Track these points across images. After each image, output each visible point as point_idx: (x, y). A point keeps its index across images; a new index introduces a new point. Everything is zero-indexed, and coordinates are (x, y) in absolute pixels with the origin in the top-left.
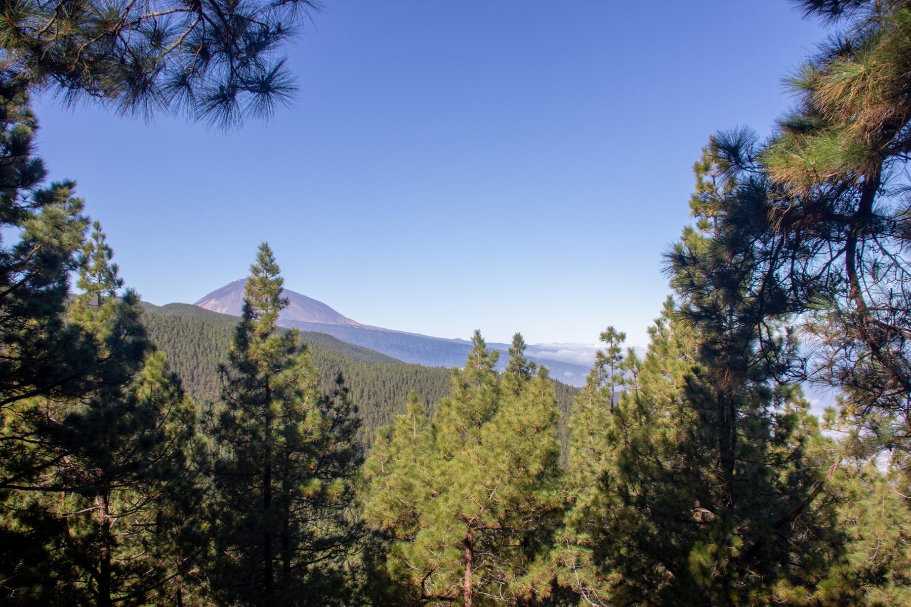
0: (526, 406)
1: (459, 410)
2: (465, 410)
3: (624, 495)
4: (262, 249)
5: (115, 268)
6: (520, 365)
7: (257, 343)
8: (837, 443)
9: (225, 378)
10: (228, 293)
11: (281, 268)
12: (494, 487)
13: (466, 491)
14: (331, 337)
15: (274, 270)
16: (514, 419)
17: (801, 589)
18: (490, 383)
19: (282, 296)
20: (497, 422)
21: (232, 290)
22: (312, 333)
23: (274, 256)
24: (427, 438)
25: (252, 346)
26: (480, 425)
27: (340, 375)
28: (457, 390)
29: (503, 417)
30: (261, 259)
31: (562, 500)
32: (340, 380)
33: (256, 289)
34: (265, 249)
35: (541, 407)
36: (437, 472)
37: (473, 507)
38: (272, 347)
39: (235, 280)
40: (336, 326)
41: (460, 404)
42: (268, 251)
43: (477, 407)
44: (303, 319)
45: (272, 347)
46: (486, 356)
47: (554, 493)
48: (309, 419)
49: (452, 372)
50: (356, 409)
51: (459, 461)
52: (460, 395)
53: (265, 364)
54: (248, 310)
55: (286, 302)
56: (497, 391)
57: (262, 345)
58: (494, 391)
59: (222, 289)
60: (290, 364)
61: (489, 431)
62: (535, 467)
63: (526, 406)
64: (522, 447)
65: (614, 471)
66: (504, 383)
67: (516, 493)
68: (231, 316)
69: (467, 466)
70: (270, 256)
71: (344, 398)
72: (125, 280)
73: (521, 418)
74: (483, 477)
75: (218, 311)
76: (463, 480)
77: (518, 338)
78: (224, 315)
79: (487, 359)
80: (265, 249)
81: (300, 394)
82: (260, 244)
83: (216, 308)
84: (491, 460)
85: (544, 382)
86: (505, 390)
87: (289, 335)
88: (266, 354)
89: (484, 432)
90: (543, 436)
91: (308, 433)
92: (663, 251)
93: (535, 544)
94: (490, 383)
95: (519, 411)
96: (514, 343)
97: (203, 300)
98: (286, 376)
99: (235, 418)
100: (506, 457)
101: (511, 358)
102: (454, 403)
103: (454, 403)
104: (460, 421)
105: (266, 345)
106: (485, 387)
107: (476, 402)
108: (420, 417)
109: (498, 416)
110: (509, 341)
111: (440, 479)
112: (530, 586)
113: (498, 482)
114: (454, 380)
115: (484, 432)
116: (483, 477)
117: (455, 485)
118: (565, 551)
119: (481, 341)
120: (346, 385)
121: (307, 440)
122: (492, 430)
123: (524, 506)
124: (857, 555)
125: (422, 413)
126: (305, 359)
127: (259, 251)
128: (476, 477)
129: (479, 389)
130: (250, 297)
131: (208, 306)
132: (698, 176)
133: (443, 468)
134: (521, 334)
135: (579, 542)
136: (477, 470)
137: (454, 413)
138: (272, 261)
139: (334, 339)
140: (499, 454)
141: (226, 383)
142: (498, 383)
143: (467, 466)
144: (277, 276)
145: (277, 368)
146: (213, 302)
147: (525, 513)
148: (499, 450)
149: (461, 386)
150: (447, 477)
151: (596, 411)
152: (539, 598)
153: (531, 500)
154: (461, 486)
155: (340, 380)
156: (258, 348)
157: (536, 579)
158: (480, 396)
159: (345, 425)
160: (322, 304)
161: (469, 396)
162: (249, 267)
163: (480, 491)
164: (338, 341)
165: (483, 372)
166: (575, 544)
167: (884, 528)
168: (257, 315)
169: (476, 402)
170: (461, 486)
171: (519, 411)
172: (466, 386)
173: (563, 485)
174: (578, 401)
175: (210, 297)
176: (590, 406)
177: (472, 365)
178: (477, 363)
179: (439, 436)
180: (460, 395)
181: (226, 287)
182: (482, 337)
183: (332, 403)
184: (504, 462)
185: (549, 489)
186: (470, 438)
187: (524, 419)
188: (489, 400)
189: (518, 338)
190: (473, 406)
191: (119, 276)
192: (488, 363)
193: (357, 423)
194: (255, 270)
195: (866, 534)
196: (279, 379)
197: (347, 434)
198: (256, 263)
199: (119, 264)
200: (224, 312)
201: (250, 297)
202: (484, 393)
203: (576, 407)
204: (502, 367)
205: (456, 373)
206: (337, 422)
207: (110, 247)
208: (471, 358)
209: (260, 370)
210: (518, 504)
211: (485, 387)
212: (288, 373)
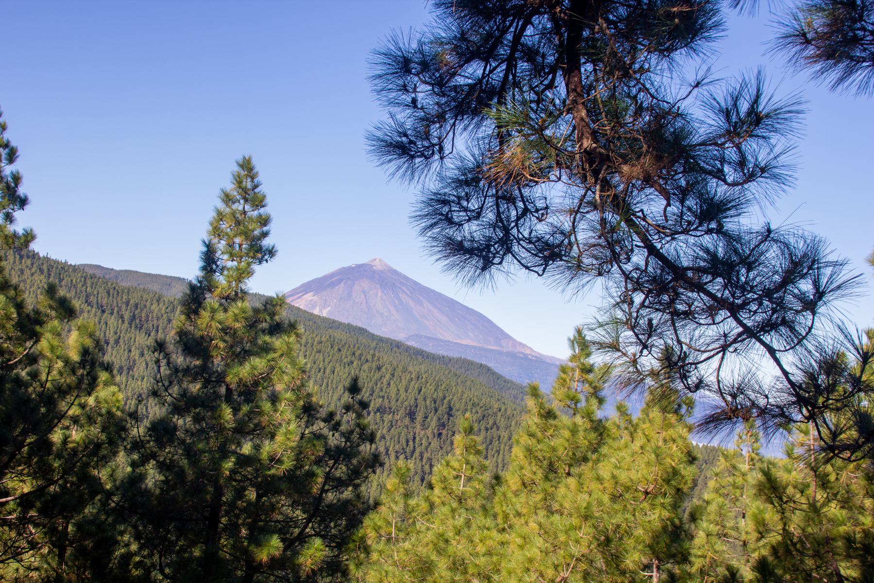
1: (529, 451)
4: (242, 166)
5: (17, 179)
7: (213, 311)
8: (570, 364)
9: (163, 363)
10: (333, 285)
11: (268, 200)
14: (489, 369)
15: (259, 202)
19: (266, 242)
21: (340, 281)
22: (458, 360)
23: (260, 178)
24: (478, 494)
25: (205, 315)
27: (355, 380)
28: (533, 421)
30: (239, 182)
32: (354, 388)
33: (224, 226)
34: (247, 166)
36: (481, 549)
38: (236, 320)
39: (347, 264)
40: (500, 353)
41: (531, 442)
42: (251, 169)
44: (448, 336)
45: (236, 320)
48: (279, 438)
49: (528, 390)
50: (372, 439)
53: (222, 345)
54: (209, 259)
55: (271, 252)
57: (221, 316)
59: (326, 278)
60: (266, 349)
61: (567, 492)
68: (334, 321)
70: (252, 178)
71: (359, 416)
72: (30, 197)
75: (316, 312)
78: (324, 320)
79: (590, 377)
80: (247, 166)
81: (274, 399)
82: (240, 158)
83: (314, 307)
87: (271, 305)
88: (225, 330)
90: (653, 506)
91: (274, 460)
97: (296, 292)
98: (254, 368)
99: (175, 428)
100: (586, 533)
105: (226, 318)
107: (560, 442)
108: (472, 458)
111: (482, 561)
114: (531, 403)
120: (364, 395)
121: (273, 471)
125: (478, 452)
126: (288, 344)
127: (236, 168)
130: (215, 241)
131: (302, 303)
133: (489, 543)
138: (256, 186)
139: (494, 373)
141: (164, 370)
144: (262, 211)
145: (242, 356)
146: (309, 296)
150: (495, 559)
155: (354, 388)
156: (212, 318)
158: (567, 434)
159: (353, 456)
160: (481, 316)
162: (218, 192)
164: (499, 377)
168: (223, 268)
172: (549, 415)
175: (306, 288)
179: (500, 490)
181: (332, 275)
183: (338, 424)
184: (582, 542)
190: (554, 449)
191: (22, 191)
193: (375, 462)
194: (228, 199)
196: (244, 371)
197: (355, 476)
198: (230, 186)
199: (23, 172)
200: (325, 313)
201: (215, 241)
205: (535, 392)
206: (337, 454)
207: (13, 144)
209: (214, 353)
212: (259, 363)
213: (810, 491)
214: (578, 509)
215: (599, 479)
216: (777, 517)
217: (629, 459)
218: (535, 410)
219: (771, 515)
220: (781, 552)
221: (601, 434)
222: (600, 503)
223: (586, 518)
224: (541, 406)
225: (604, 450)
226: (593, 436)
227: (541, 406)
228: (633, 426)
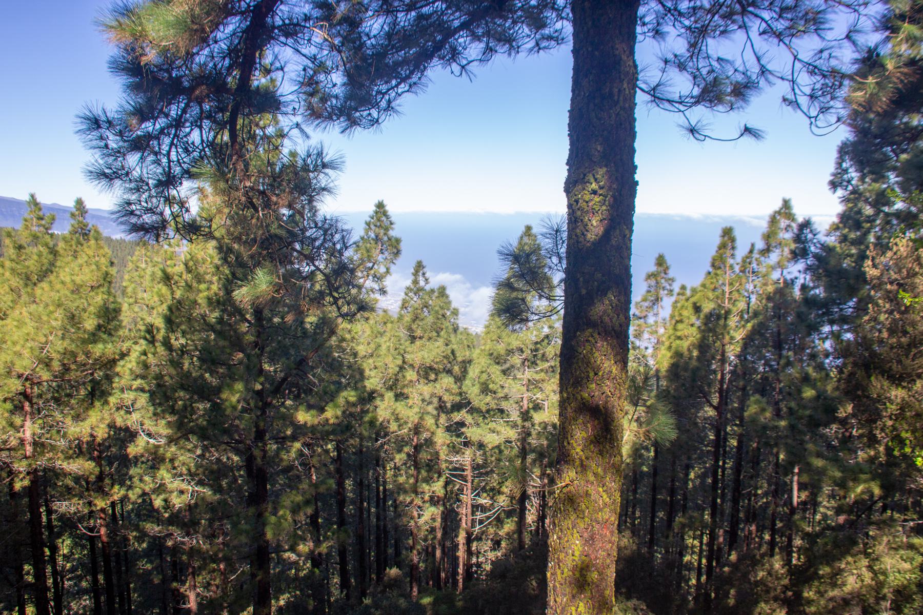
0: (81, 266)
1: (13, 270)
2: (19, 271)
3: (167, 344)
6: (82, 229)
12: (46, 343)
13: (18, 348)
16: (68, 279)
17: (313, 412)
18: (46, 245)
20: (51, 282)
26: (35, 284)
28: (12, 252)
29: (57, 277)
31: (118, 351)
35: (94, 267)
37: (26, 362)
41: (14, 265)
43: (33, 268)
46: (42, 219)
47: (110, 346)
51: (14, 320)
52: (14, 257)
56: (54, 252)
58: (51, 253)
61: (43, 290)
62: (90, 324)
63: (81, 266)
64: (76, 305)
65: (159, 322)
66: (61, 245)
67: (73, 347)
69: (21, 324)
73: (74, 278)
74: (36, 334)
76: (15, 338)
77: (80, 202)
79: (43, 222)
84: (45, 318)
85: (98, 244)
86: (62, 252)
89: (38, 292)
90: (97, 294)
92: (77, 113)
93: (98, 393)
94: (46, 245)
95: (77, 270)
96: (75, 207)
100: (59, 314)
101: (73, 222)
102: (8, 264)
103: (8, 264)
104: (16, 282)
106: (41, 249)
109: (52, 277)
110: (70, 204)
112: (89, 431)
113: (51, 338)
115: (38, 292)
116: (36, 334)
117: (9, 343)
118: (122, 396)
119: (36, 204)
122: (46, 289)
123: (81, 358)
124: (371, 380)
128: (28, 334)
129: (35, 250)
132: (839, 164)
134: (83, 199)
135: (134, 387)
136: (30, 327)
137: (8, 274)
140: (52, 312)
142: (56, 245)
143: (21, 324)
147: (84, 365)
148: (51, 308)
149: (15, 248)
151: (149, 271)
152: (99, 440)
153: (88, 354)
154: (15, 343)
157: (95, 423)
158: (35, 257)
161: (23, 257)
163: (31, 348)
165: (40, 235)
166: (130, 389)
167: (391, 358)
169: (32, 264)
170: (15, 343)
171: (77, 270)
172: (20, 248)
173: (120, 337)
174: (132, 262)
176: (143, 266)
177: (27, 227)
178: (32, 225)
180: (14, 257)
182: (38, 200)
184: (58, 319)
185: (105, 342)
186: (25, 298)
187: (78, 280)
188: (45, 261)
189: (80, 202)
190: (28, 267)
192: (44, 226)
195: (378, 364)
202: (40, 255)
203: (130, 266)
204: (62, 229)
208: (26, 221)
210: (76, 357)
211: (41, 249)
213: (184, 277)
214: (53, 301)
215: (63, 283)
216: (169, 293)
217: (77, 269)
218: (11, 246)
219: (164, 290)
220: (174, 310)
221: (55, 255)
222: (66, 296)
223: (59, 306)
224: (15, 242)
225: (58, 264)
226: (51, 257)
227: (15, 242)
228: (395, 512)
